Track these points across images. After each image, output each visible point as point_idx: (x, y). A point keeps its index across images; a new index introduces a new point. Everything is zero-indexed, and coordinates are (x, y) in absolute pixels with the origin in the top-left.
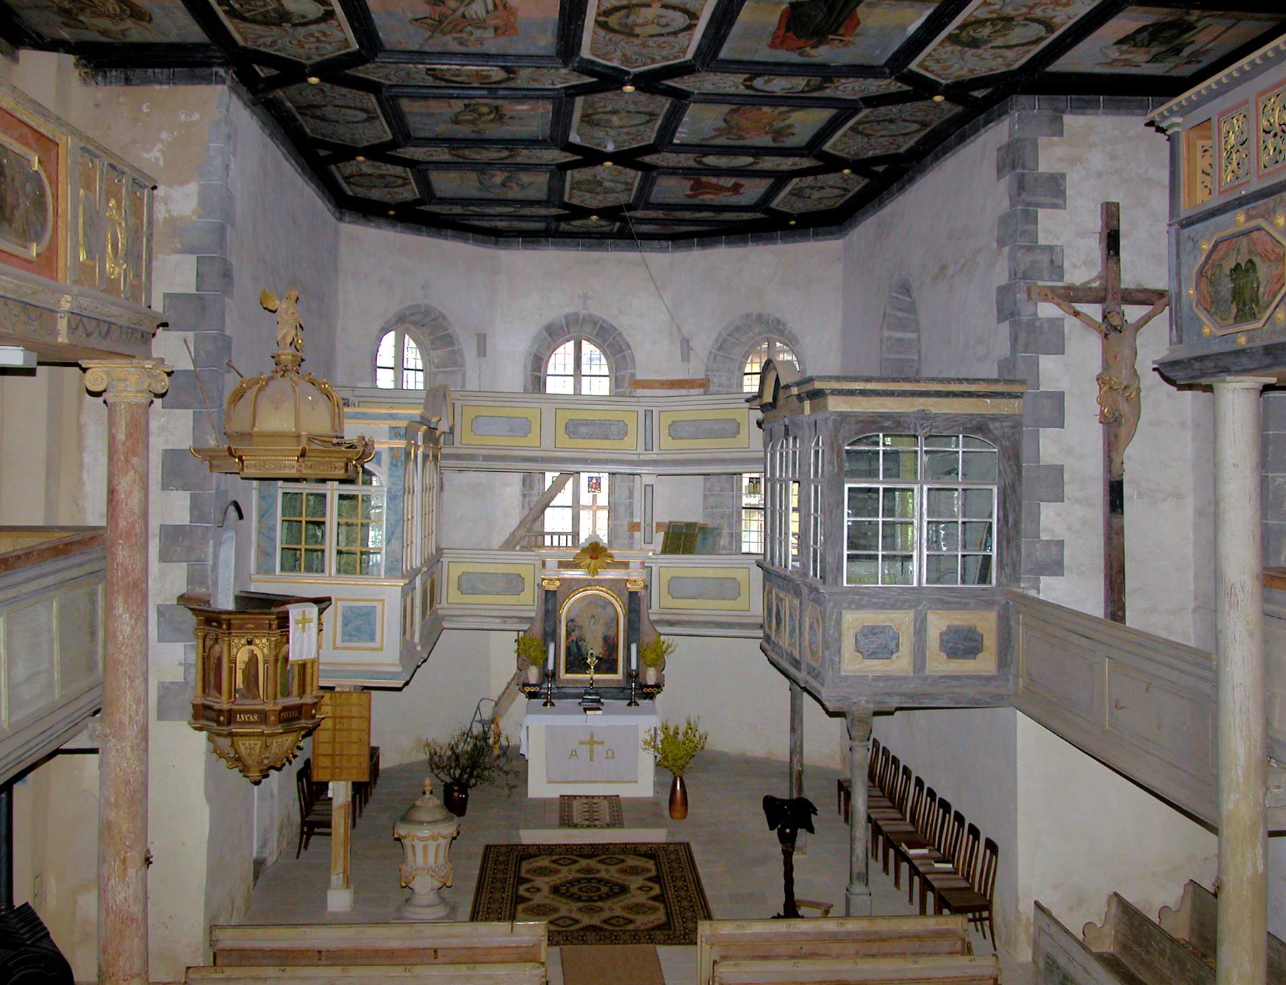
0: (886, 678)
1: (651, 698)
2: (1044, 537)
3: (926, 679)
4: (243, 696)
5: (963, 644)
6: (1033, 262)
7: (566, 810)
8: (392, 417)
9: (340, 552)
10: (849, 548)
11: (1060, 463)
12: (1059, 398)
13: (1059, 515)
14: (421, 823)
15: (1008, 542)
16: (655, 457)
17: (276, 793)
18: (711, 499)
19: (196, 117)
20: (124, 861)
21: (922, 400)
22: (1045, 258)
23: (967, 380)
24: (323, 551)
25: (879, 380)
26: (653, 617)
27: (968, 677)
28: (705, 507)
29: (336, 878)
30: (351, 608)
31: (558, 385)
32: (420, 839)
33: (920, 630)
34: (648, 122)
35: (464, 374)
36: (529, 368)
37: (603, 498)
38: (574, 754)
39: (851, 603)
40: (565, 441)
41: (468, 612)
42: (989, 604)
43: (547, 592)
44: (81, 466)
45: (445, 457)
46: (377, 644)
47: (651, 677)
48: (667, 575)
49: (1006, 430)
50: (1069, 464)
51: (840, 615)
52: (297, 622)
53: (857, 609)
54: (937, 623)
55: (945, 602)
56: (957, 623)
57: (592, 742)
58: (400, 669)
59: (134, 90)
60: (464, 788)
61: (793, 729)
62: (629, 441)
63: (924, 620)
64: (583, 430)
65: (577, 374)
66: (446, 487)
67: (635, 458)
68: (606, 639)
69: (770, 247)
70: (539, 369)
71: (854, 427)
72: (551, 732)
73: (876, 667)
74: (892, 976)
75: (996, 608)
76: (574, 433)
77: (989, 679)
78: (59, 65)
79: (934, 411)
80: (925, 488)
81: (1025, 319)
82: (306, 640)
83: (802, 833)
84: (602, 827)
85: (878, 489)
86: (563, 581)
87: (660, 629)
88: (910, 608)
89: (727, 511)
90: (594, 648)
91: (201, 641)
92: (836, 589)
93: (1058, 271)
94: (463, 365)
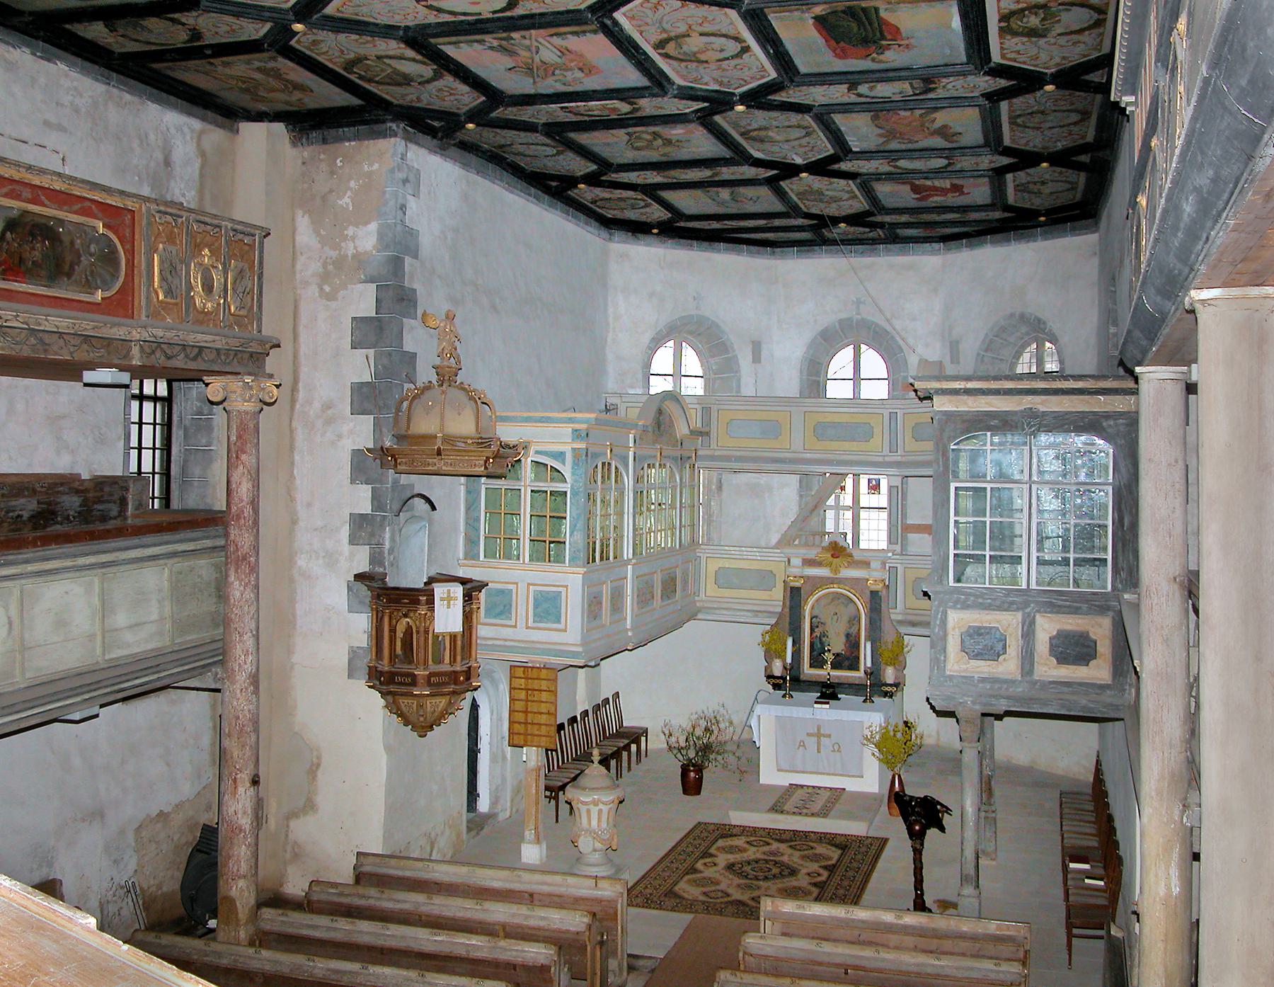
0: (994, 680)
1: (891, 697)
7: (782, 800)
14: (584, 789)
15: (1124, 546)
19: (376, 166)
20: (235, 781)
21: (1030, 398)
23: (1072, 377)
25: (980, 379)
27: (1081, 684)
29: (529, 834)
31: (838, 390)
33: (1028, 633)
34: (1082, 120)
35: (739, 380)
36: (805, 373)
37: (882, 499)
39: (957, 602)
44: (292, 463)
46: (561, 626)
47: (889, 675)
49: (1122, 428)
51: (945, 614)
52: (442, 599)
53: (962, 608)
54: (1047, 627)
55: (1056, 603)
56: (1069, 627)
57: (819, 735)
59: (331, 148)
60: (699, 769)
62: (876, 442)
63: (1033, 622)
65: (857, 378)
66: (724, 487)
67: (881, 459)
68: (848, 636)
69: (1032, 245)
70: (818, 374)
73: (982, 668)
74: (912, 968)
75: (1111, 614)
77: (1103, 687)
78: (268, 132)
79: (1042, 409)
83: (932, 833)
84: (806, 815)
85: (985, 489)
86: (807, 579)
87: (903, 630)
88: (1018, 609)
90: (837, 644)
94: (738, 371)
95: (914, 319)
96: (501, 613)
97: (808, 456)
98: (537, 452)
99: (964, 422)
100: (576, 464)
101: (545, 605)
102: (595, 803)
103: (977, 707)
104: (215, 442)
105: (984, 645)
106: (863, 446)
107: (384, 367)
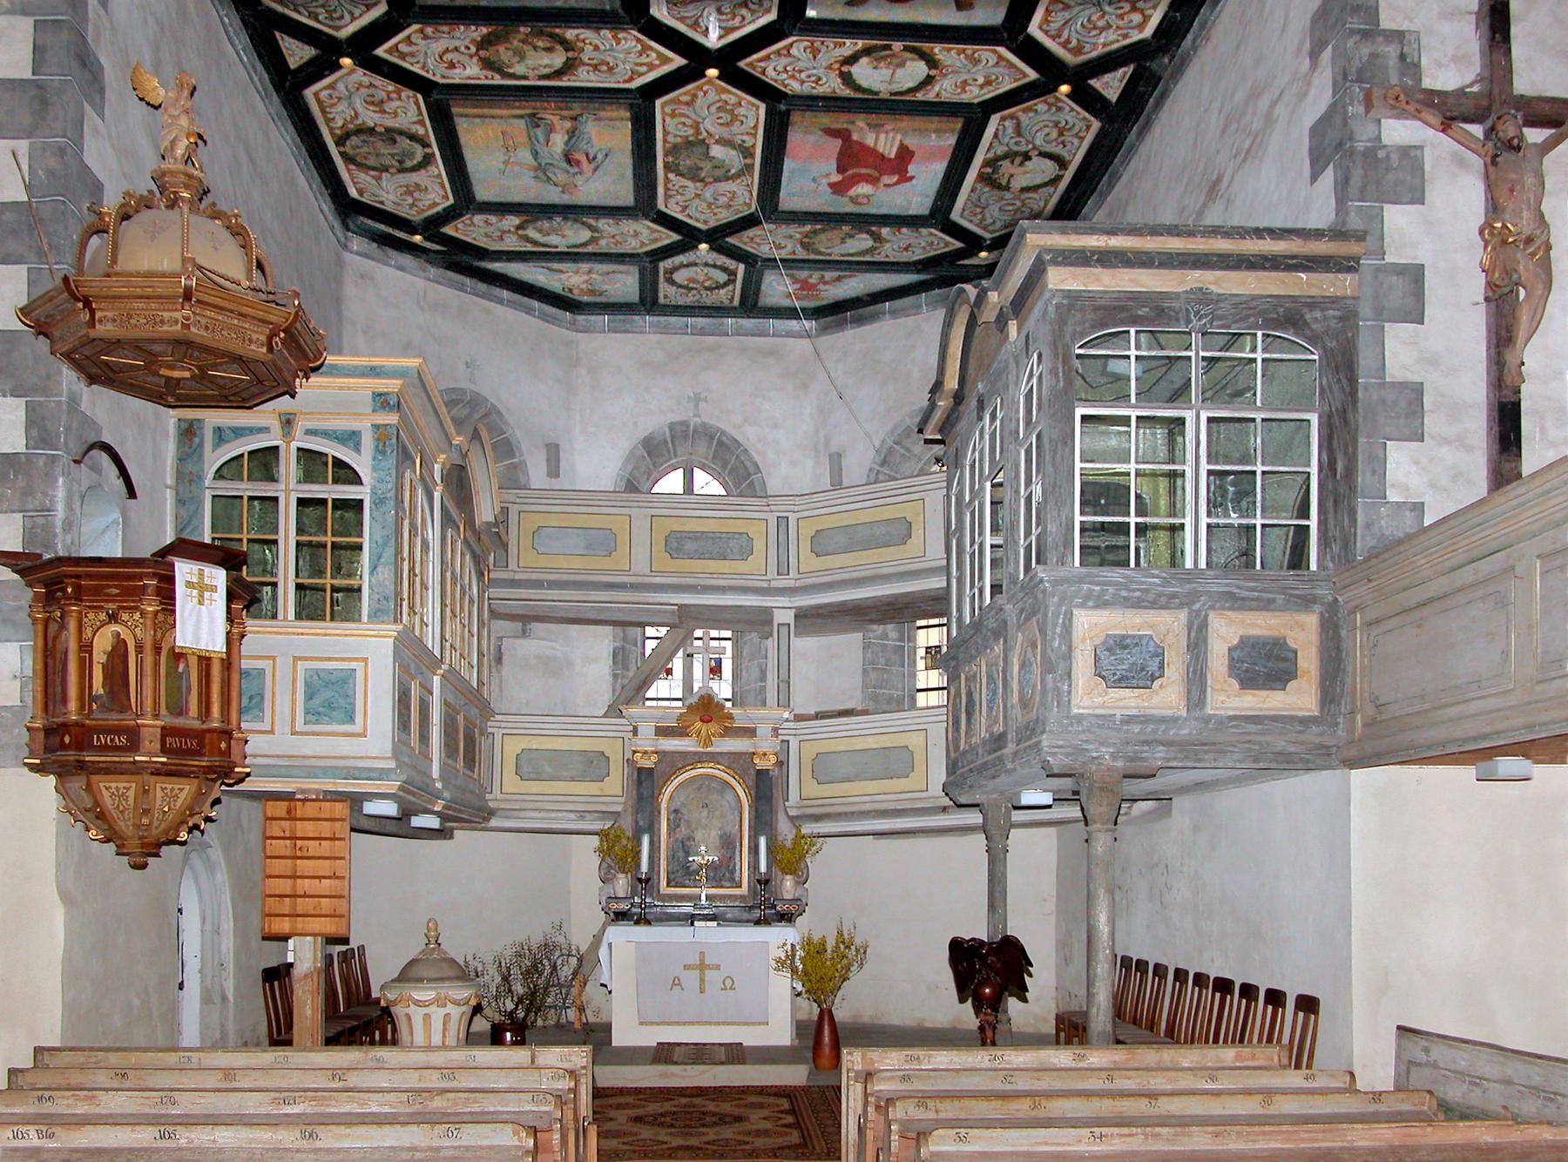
0: (1146, 720)
2: (1393, 496)
3: (1207, 720)
4: (103, 708)
5: (1265, 665)
6: (1373, 55)
8: (374, 372)
9: (299, 587)
10: (1082, 513)
11: (1417, 379)
12: (1415, 275)
13: (1416, 463)
14: (420, 980)
15: (1336, 502)
16: (791, 583)
17: (231, 996)
18: (873, 675)
22: (1392, 51)
24: (274, 585)
26: (793, 813)
27: (1274, 718)
28: (865, 686)
30: (317, 671)
32: (418, 1003)
33: (1197, 644)
38: (676, 982)
39: (1087, 598)
40: (664, 562)
41: (531, 805)
42: (1306, 602)
43: (640, 770)
45: (494, 583)
46: (357, 727)
48: (810, 751)
49: (1333, 323)
50: (1434, 383)
51: (1069, 617)
53: (1096, 607)
54: (1225, 631)
57: (702, 967)
58: (392, 764)
61: (992, 906)
62: (755, 563)
63: (1204, 625)
64: (689, 546)
66: (505, 658)
67: (765, 585)
71: (1090, 316)
72: (644, 955)
73: (1127, 701)
75: (1317, 608)
76: (678, 550)
77: (1305, 721)
80: (1204, 416)
81: (1360, 146)
82: (205, 619)
88: (1181, 606)
89: (896, 694)
91: (40, 628)
92: (1063, 572)
93: (1411, 67)
95: (776, 426)
97: (658, 580)
98: (309, 432)
99: (1096, 309)
100: (380, 451)
101: (327, 694)
102: (440, 1002)
103: (1120, 764)
105: (1130, 664)
106: (741, 566)
107: (51, 173)
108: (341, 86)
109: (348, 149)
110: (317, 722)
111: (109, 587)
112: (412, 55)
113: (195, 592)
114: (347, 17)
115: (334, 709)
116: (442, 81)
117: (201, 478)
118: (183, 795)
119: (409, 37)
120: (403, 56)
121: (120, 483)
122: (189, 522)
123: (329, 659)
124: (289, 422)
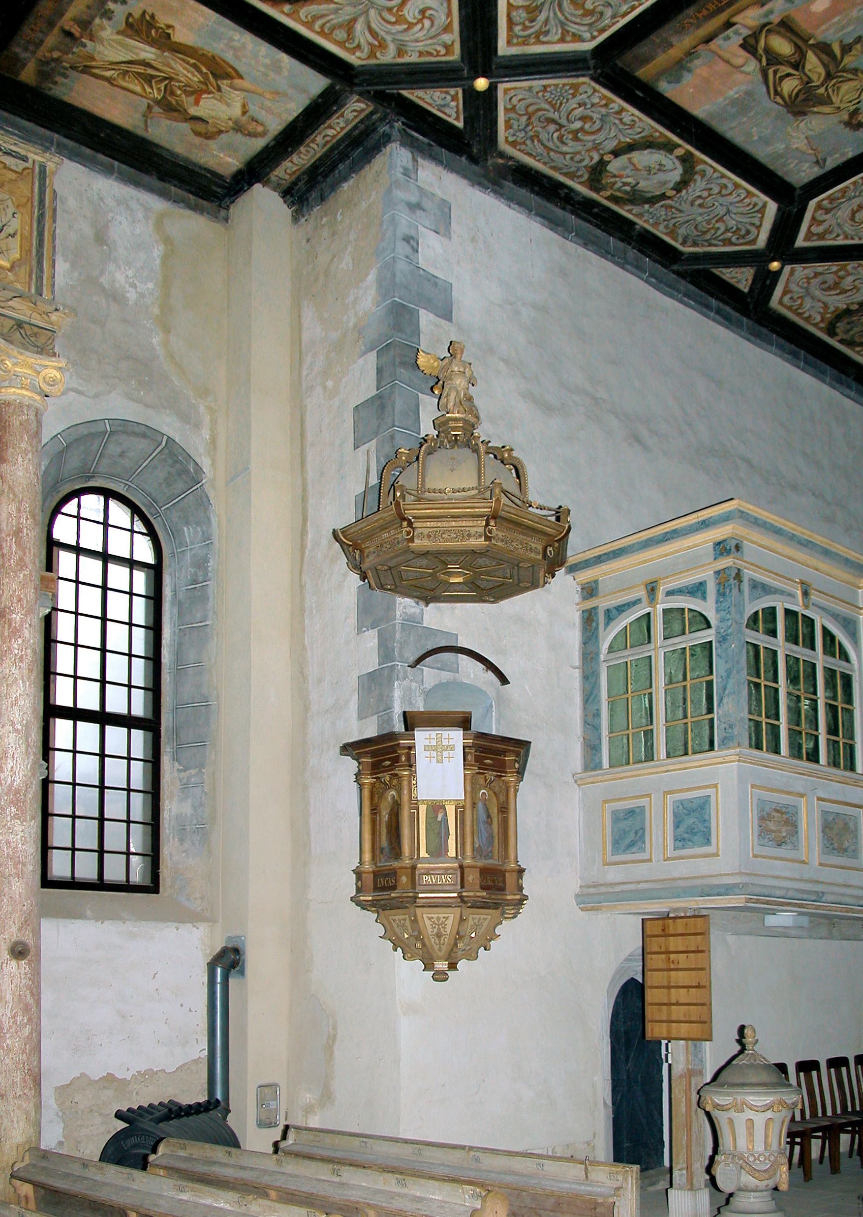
30: (681, 802)
96: (632, 844)
98: (670, 593)
101: (689, 821)
104: (210, 614)
108: (793, 287)
109: (841, 336)
110: (683, 847)
111: (487, 758)
112: (828, 231)
113: (445, 754)
114: (753, 230)
115: (695, 834)
116: (687, 250)
117: (597, 654)
118: (449, 922)
119: (813, 218)
120: (821, 236)
121: (490, 675)
122: (591, 693)
123: (689, 790)
124: (653, 589)
